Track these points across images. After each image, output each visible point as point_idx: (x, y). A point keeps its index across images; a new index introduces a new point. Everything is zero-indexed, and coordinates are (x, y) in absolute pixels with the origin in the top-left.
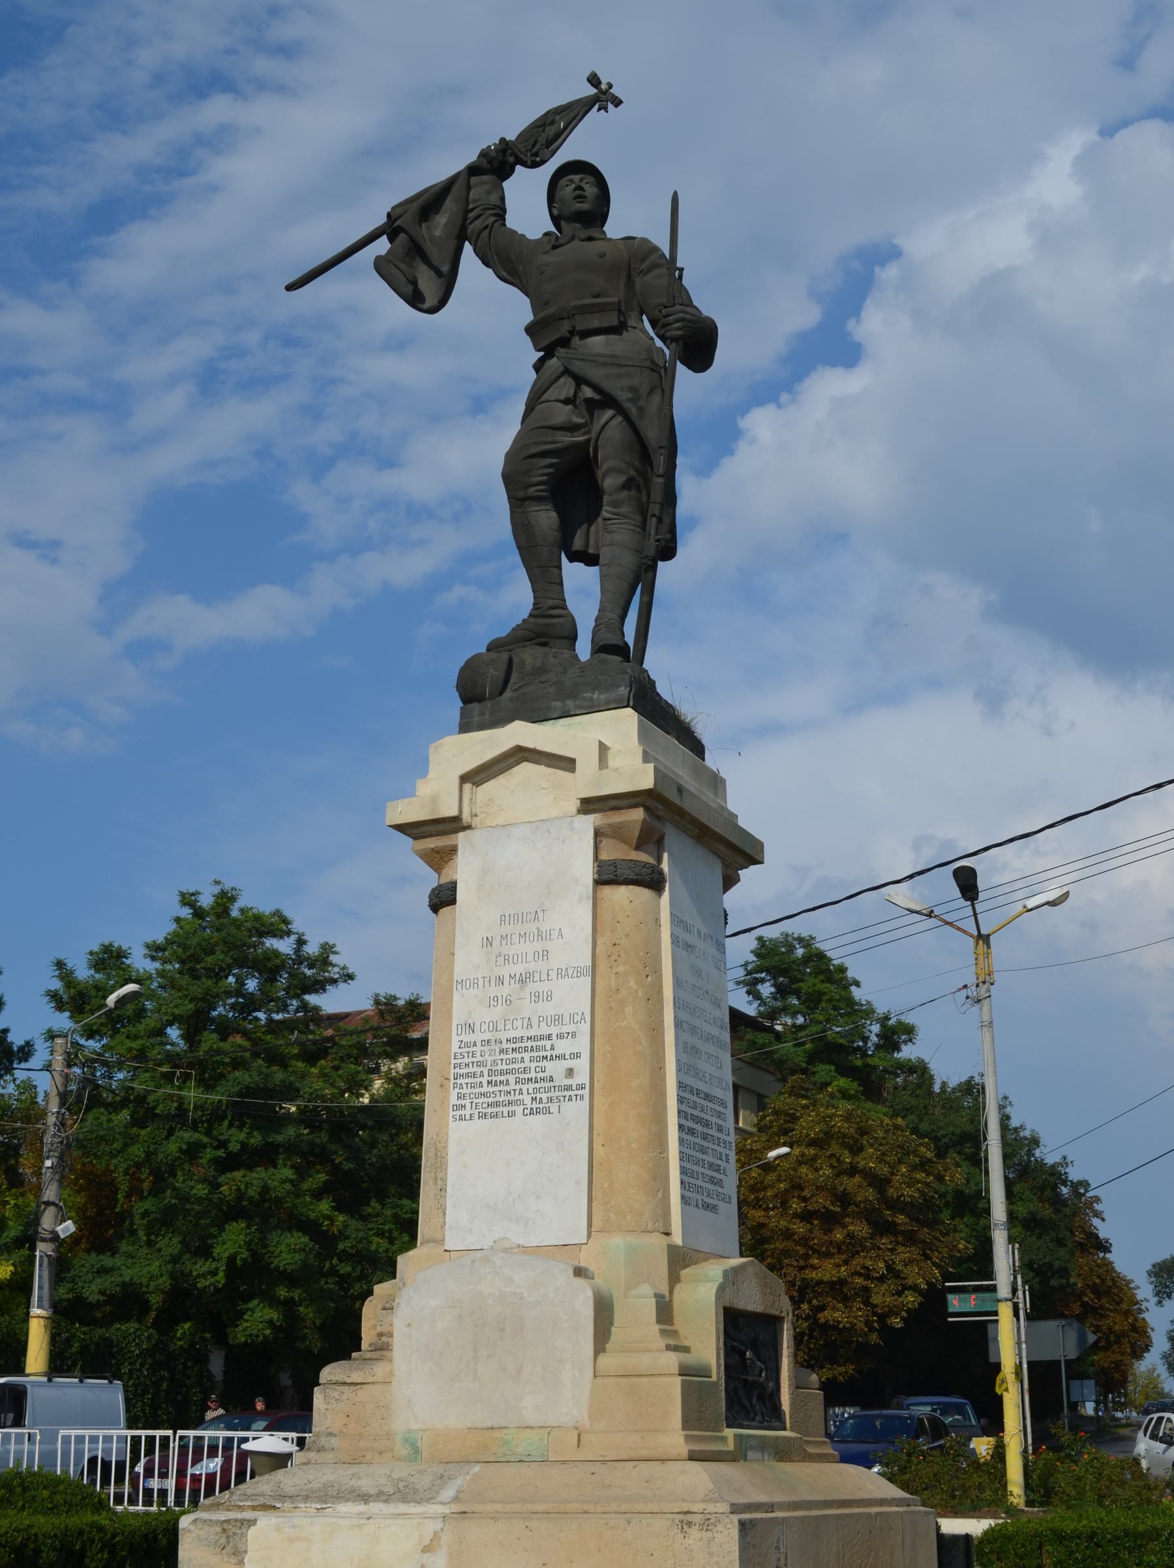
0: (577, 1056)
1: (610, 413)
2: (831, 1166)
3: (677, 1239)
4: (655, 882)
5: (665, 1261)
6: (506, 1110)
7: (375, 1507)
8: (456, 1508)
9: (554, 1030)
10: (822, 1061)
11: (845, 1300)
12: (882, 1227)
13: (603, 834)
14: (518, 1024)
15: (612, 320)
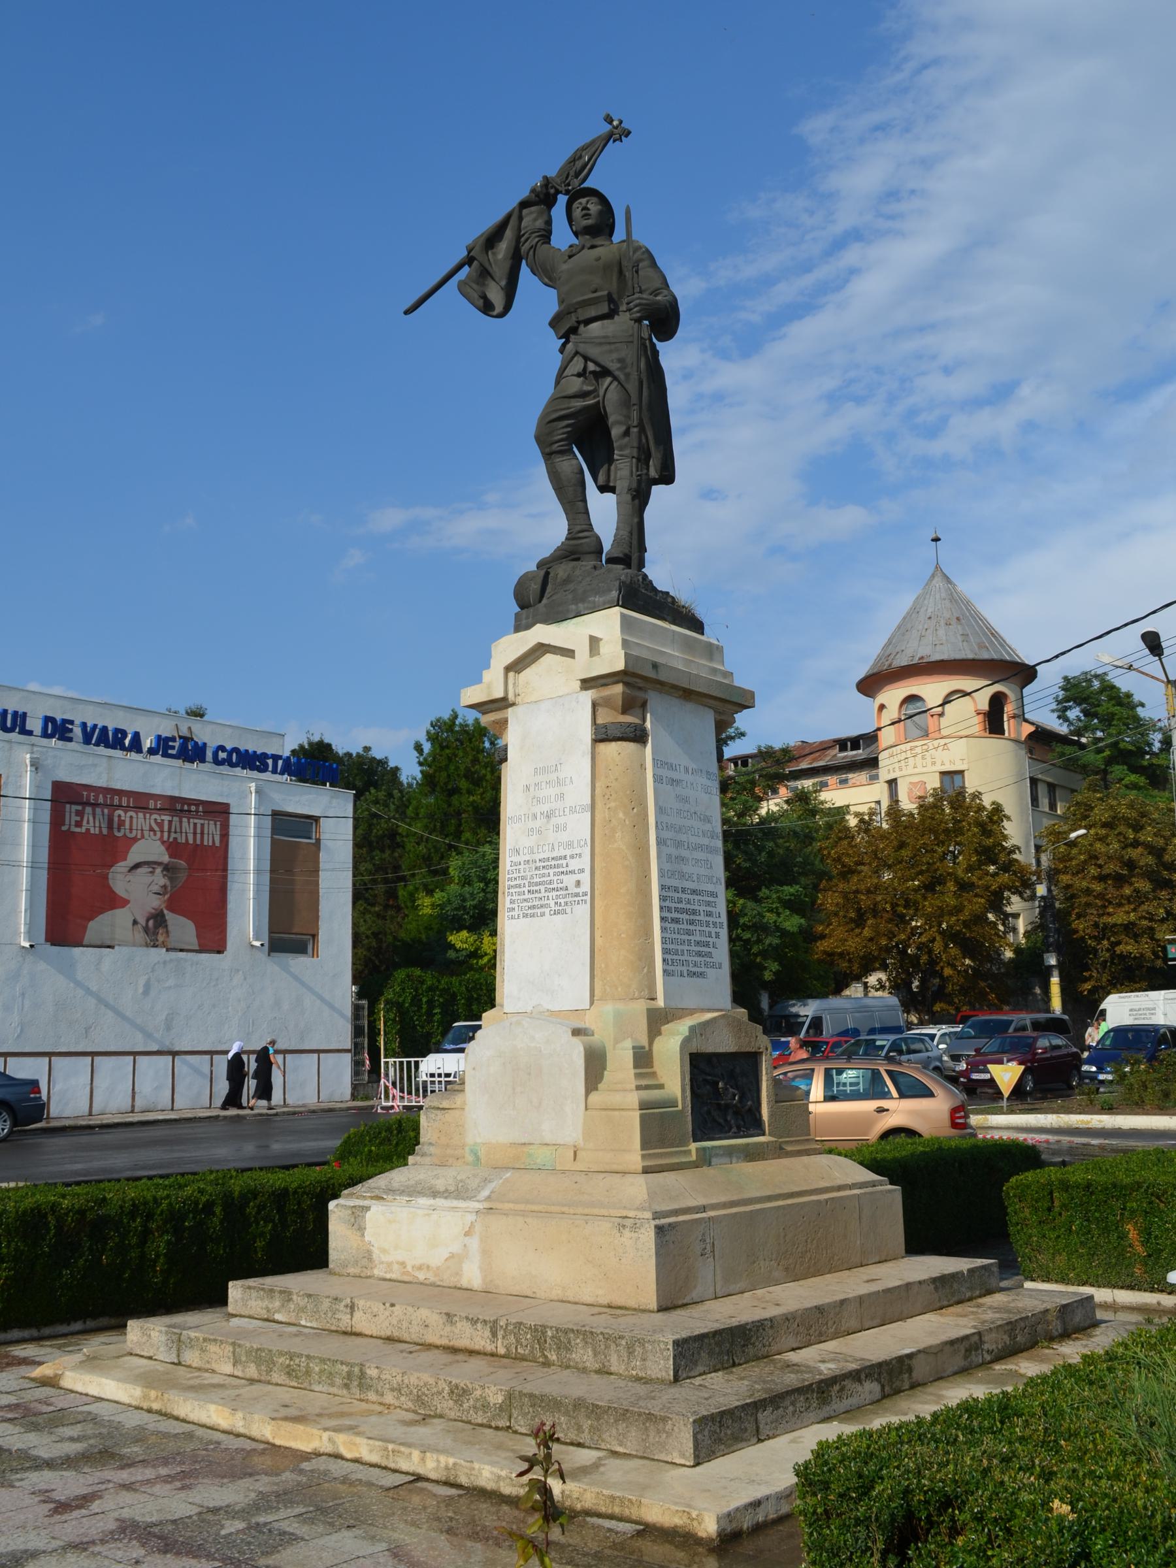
0: (582, 871)
1: (609, 379)
2: (1119, 841)
3: (661, 1003)
4: (638, 736)
5: (645, 1021)
6: (539, 911)
7: (440, 1202)
8: (487, 1205)
9: (568, 852)
10: (1118, 764)
11: (1136, 937)
12: (1161, 884)
13: (599, 705)
14: (546, 848)
15: (604, 308)
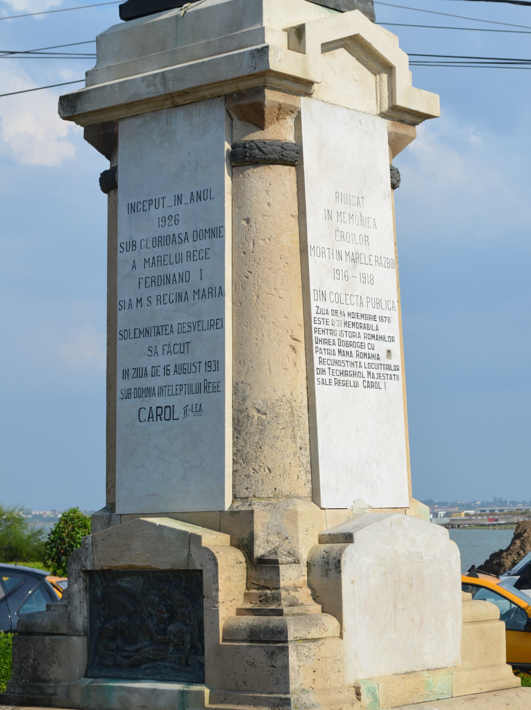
6: (352, 379)
14: (354, 300)
